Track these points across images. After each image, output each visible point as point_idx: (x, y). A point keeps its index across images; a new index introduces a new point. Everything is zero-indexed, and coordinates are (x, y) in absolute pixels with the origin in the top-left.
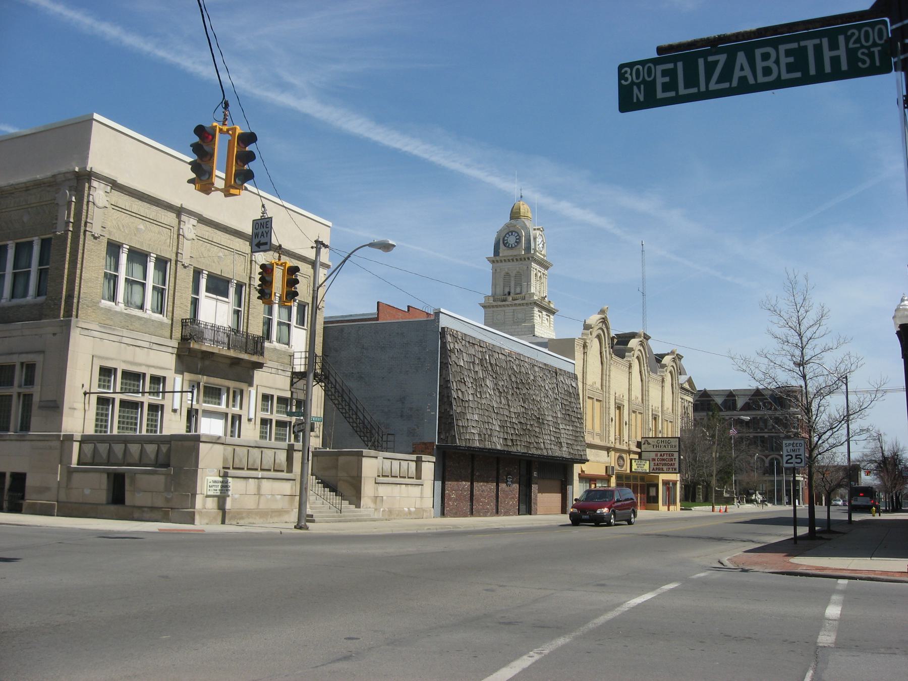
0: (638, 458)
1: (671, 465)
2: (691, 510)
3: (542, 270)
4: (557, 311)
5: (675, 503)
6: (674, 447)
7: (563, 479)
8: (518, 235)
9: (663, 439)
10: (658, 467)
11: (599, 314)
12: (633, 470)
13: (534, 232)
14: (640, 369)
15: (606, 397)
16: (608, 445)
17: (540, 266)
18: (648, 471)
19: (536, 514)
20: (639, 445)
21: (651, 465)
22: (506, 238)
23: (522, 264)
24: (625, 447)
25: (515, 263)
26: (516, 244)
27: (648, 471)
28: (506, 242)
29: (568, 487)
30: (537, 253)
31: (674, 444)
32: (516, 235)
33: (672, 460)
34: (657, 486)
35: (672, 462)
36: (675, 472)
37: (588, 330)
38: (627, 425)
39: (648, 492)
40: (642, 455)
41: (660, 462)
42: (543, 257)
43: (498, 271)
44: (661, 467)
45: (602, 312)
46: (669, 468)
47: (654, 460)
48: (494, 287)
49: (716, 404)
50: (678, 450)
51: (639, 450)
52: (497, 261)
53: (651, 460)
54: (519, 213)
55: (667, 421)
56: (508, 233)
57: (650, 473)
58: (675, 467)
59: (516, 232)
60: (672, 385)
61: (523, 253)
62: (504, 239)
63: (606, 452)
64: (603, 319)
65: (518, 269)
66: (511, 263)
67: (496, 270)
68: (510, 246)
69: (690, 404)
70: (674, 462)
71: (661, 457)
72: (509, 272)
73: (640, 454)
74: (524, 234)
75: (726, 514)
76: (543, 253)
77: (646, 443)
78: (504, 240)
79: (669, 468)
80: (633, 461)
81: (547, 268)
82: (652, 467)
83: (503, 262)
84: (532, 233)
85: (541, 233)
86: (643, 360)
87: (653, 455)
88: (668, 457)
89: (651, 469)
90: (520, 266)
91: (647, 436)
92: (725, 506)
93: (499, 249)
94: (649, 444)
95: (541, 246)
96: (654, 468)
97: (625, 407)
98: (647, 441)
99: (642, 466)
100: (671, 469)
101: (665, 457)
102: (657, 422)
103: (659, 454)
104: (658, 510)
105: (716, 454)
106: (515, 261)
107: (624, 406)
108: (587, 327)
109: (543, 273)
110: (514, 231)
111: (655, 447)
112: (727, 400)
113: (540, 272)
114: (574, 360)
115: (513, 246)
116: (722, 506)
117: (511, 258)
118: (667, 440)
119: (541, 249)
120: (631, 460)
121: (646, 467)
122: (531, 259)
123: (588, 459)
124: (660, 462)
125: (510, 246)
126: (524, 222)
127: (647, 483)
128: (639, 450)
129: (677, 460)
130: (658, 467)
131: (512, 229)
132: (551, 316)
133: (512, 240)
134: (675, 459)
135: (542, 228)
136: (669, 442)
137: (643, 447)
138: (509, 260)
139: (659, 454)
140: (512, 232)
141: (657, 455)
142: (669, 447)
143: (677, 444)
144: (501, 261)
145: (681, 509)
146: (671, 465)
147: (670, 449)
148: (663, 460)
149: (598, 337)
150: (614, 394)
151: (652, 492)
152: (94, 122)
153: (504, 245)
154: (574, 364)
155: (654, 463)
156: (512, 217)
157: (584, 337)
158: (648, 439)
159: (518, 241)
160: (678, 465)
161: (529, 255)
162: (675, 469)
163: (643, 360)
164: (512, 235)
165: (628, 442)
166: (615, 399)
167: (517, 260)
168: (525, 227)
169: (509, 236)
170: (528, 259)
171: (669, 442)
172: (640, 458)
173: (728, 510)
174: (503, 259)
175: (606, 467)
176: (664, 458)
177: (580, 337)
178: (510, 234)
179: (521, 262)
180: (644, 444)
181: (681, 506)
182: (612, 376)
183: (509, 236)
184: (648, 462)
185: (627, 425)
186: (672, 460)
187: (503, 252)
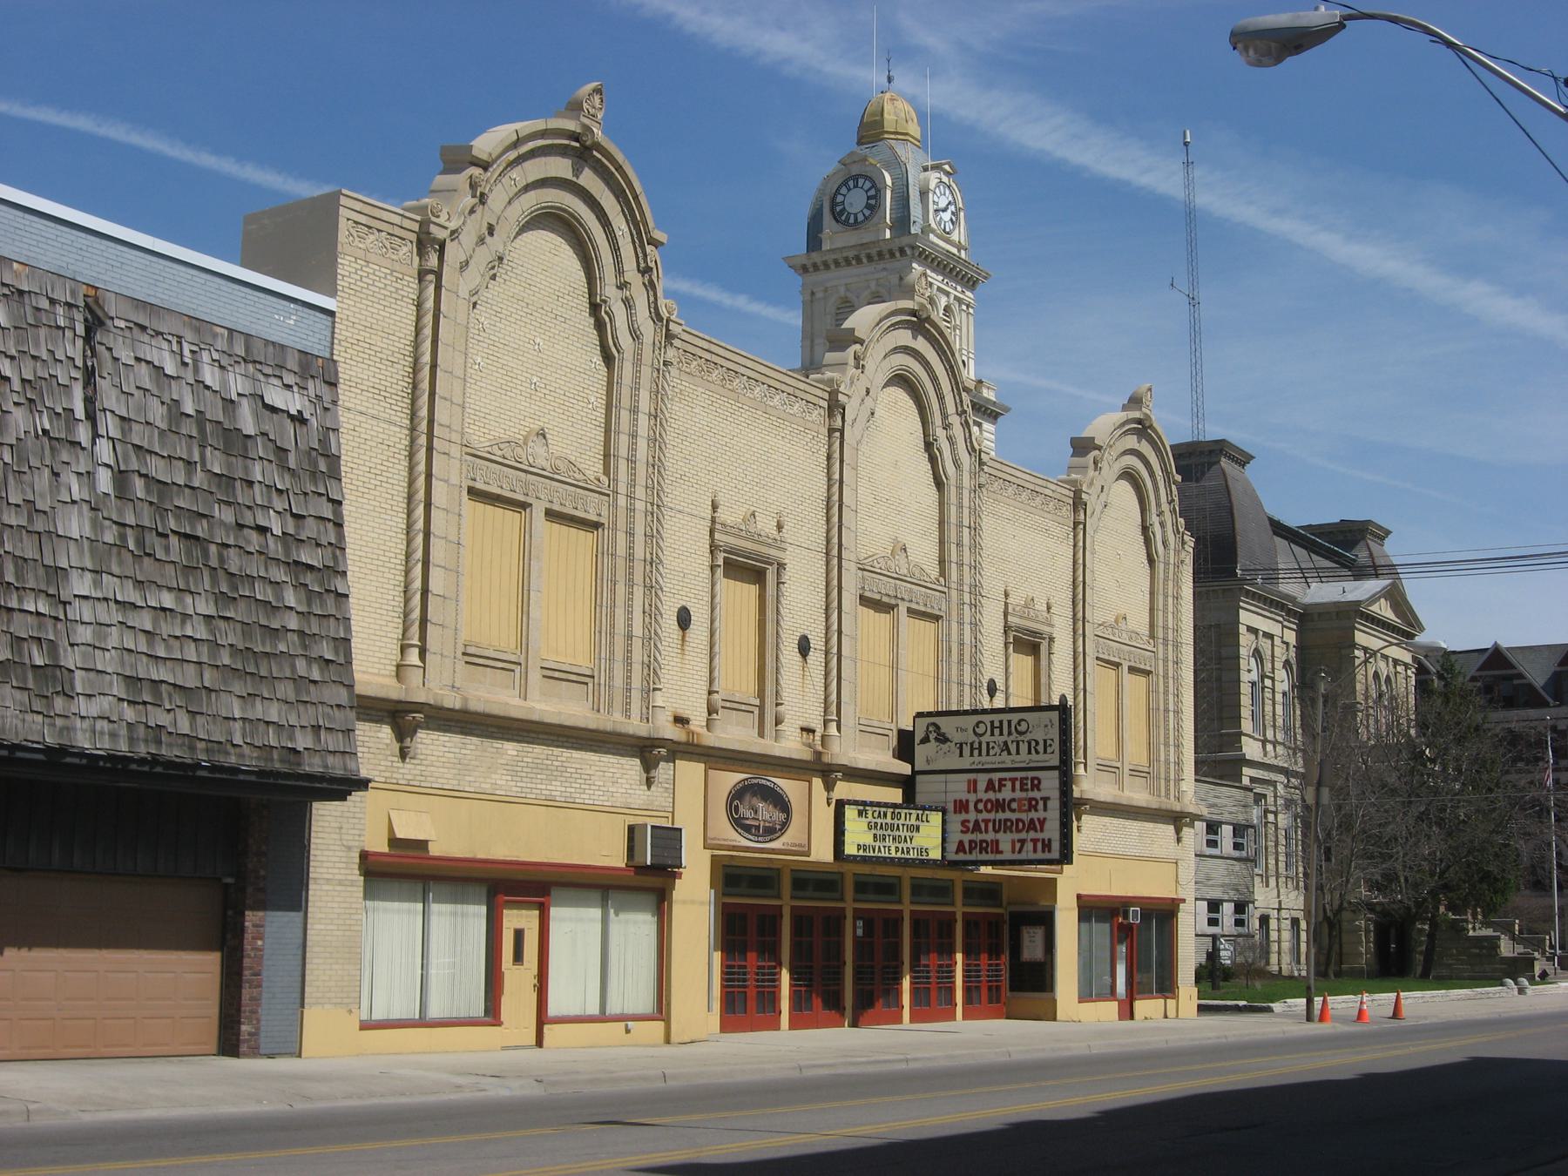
0: (899, 800)
1: (1031, 826)
2: (1269, 1010)
3: (956, 290)
4: (1007, 410)
5: (1166, 986)
6: (1041, 748)
7: (229, 880)
8: (874, 186)
9: (996, 718)
10: (978, 837)
11: (1125, 408)
12: (850, 849)
13: (923, 175)
14: (926, 434)
15: (1166, 660)
16: (1177, 807)
17: (943, 274)
18: (936, 854)
19: (255, 1052)
20: (905, 746)
21: (949, 827)
22: (839, 199)
23: (885, 269)
24: (790, 745)
25: (867, 268)
26: (867, 212)
27: (936, 854)
28: (838, 209)
29: (251, 918)
30: (932, 237)
31: (1039, 735)
32: (868, 185)
33: (1032, 805)
34: (1046, 920)
35: (1033, 815)
36: (1047, 856)
37: (459, 171)
38: (816, 657)
39: (1016, 950)
40: (919, 788)
41: (985, 815)
42: (955, 251)
43: (819, 295)
44: (990, 836)
45: (1135, 401)
46: (1023, 842)
47: (961, 806)
48: (808, 343)
49: (1530, 687)
50: (1055, 761)
51: (905, 769)
52: (816, 267)
53: (950, 807)
54: (881, 123)
55: (1117, 665)
56: (845, 183)
57: (945, 863)
58: (1045, 835)
59: (867, 178)
60: (1145, 529)
61: (888, 235)
62: (833, 200)
63: (1172, 827)
64: (1139, 421)
65: (873, 285)
66: (854, 270)
67: (813, 294)
68: (852, 221)
69: (1400, 669)
70: (1041, 814)
71: (991, 795)
72: (849, 295)
73: (908, 784)
74: (889, 181)
75: (1395, 1023)
76: (955, 237)
77: (932, 736)
78: (833, 204)
79: (1023, 842)
80: (850, 813)
81: (970, 283)
82: (956, 836)
83: (833, 267)
84: (915, 178)
85: (945, 179)
86: (941, 398)
87: (957, 787)
88: (1018, 794)
89: (952, 847)
90: (877, 276)
91: (954, 708)
92: (1393, 995)
93: (821, 231)
94: (943, 739)
95: (946, 216)
96: (961, 843)
97: (1056, 646)
98: (937, 727)
99: (903, 833)
100: (1030, 846)
101: (1006, 794)
102: (1044, 662)
103: (982, 780)
104: (1055, 1019)
105: (1318, 790)
106: (865, 260)
107: (1051, 639)
108: (1082, 446)
109: (956, 298)
110: (861, 176)
111: (966, 750)
112: (1561, 672)
113: (947, 294)
114: (332, 292)
115: (861, 217)
116: (1366, 997)
117: (851, 254)
118: (1015, 717)
119: (949, 227)
120: (840, 806)
121: (928, 838)
122: (909, 252)
123: (364, 773)
124: (985, 815)
125: (852, 221)
126: (891, 148)
127: (1013, 908)
128: (905, 769)
129: (1054, 804)
130: (978, 837)
131: (855, 170)
132: (986, 426)
133: (855, 201)
134: (1045, 800)
135: (948, 163)
136: (1023, 727)
137: (921, 752)
138: (848, 262)
139: (982, 780)
140: (856, 178)
141: (973, 787)
142: (1024, 748)
143: (1054, 734)
144: (826, 266)
145: (1202, 1009)
146: (1031, 826)
147: (1024, 758)
148: (999, 805)
149: (1129, 475)
150: (708, 513)
151: (1032, 949)
152: (341, 197)
153: (835, 218)
154: (331, 314)
155: (964, 823)
156: (863, 137)
157: (1074, 476)
158: (941, 721)
159: (872, 202)
160: (1057, 824)
161: (905, 240)
162: (1047, 845)
163: (941, 398)
164: (856, 186)
165: (817, 725)
166: (1006, 614)
167: (870, 258)
168: (896, 165)
169: (849, 190)
170: (902, 251)
171: (1023, 727)
172: (909, 799)
173: (1405, 1012)
174: (830, 258)
175: (631, 829)
176: (1000, 796)
177: (1064, 477)
178: (851, 183)
179: (881, 265)
180: (925, 740)
181: (1199, 999)
182: (987, 540)
183: (849, 190)
184: (936, 818)
185: (816, 657)
186: (1032, 805)
187: (834, 238)
